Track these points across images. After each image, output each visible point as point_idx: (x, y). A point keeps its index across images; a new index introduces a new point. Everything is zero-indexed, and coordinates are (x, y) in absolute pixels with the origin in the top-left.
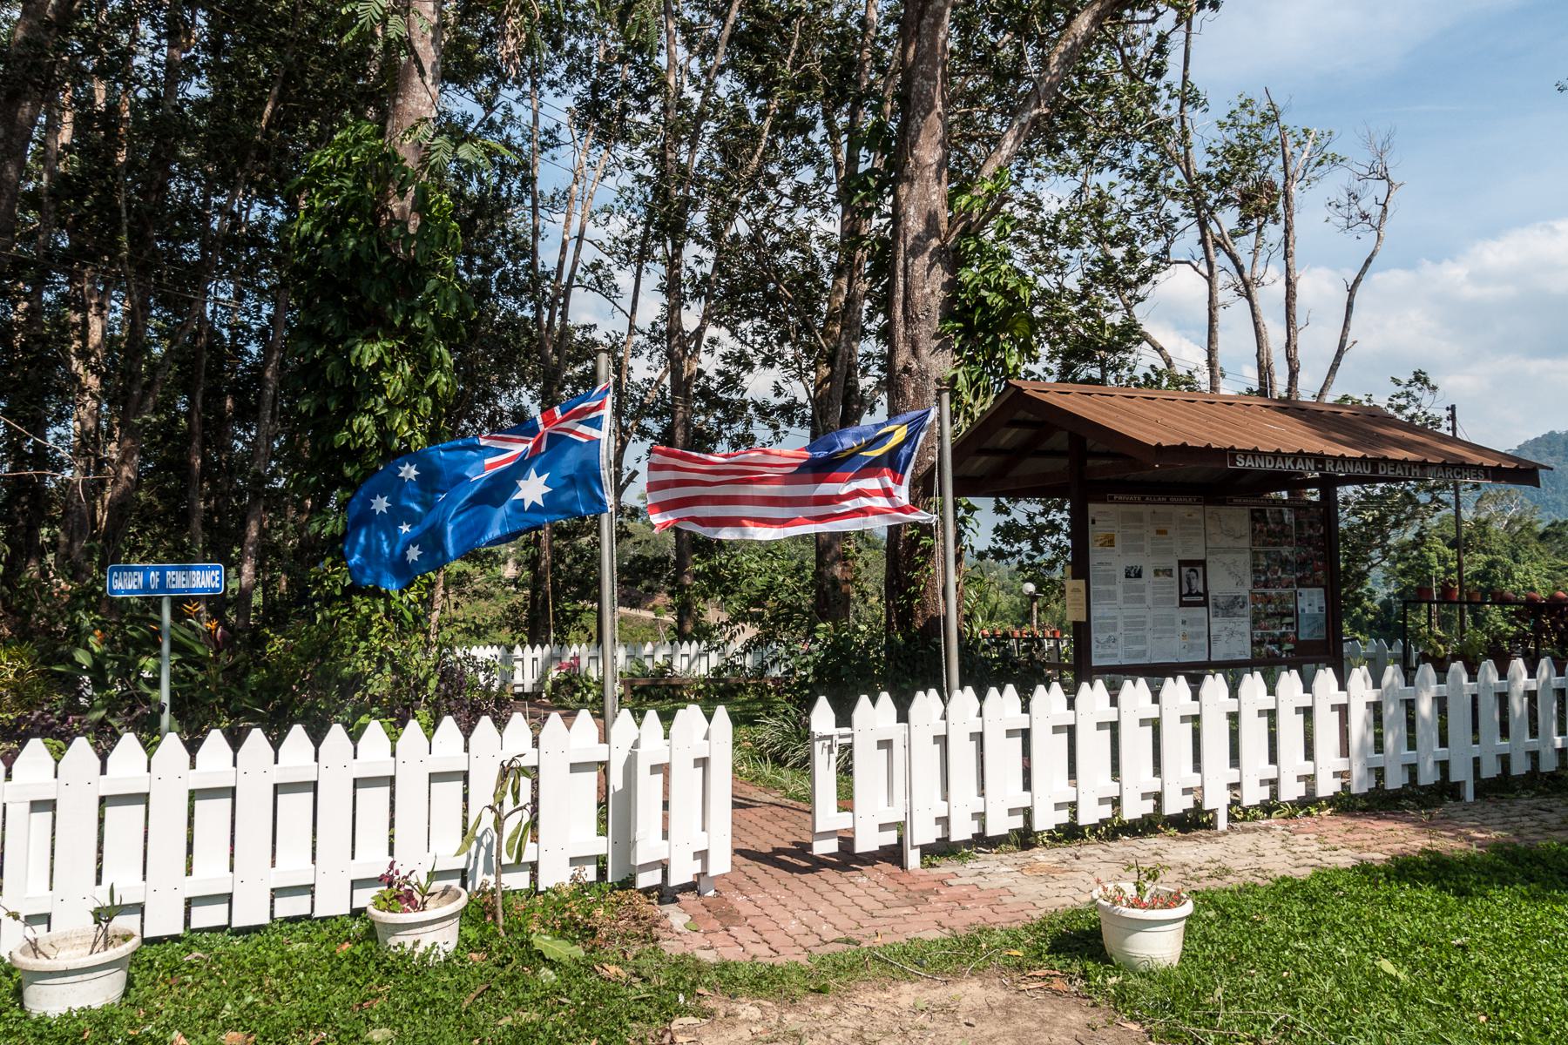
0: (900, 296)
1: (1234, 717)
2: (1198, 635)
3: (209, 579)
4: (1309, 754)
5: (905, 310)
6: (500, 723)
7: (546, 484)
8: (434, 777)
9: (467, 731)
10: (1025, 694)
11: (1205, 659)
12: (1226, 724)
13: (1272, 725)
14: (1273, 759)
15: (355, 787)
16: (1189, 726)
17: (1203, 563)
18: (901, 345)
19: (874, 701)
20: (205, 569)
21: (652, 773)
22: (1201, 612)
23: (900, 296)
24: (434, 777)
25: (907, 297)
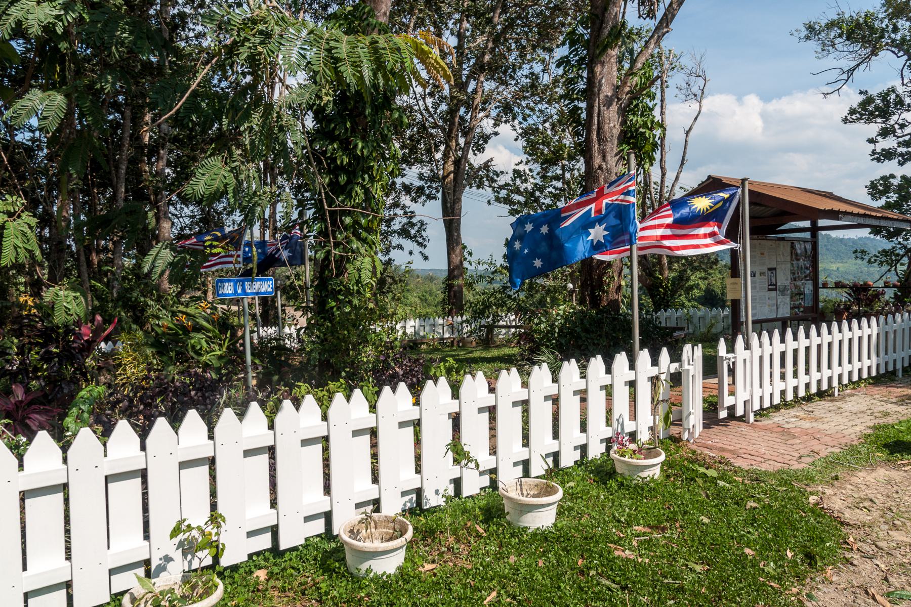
0: (595, 127)
1: (456, 420)
2: (773, 305)
3: (267, 286)
4: (584, 428)
5: (598, 135)
6: (176, 421)
7: (605, 229)
8: (183, 465)
9: (143, 433)
10: (416, 389)
11: (774, 316)
12: (450, 422)
13: (526, 412)
14: (556, 435)
15: (22, 500)
16: (519, 409)
17: (775, 269)
18: (596, 155)
19: (394, 389)
20: (265, 280)
21: (545, 400)
22: (774, 293)
23: (595, 127)
24: (183, 465)
25: (599, 128)
